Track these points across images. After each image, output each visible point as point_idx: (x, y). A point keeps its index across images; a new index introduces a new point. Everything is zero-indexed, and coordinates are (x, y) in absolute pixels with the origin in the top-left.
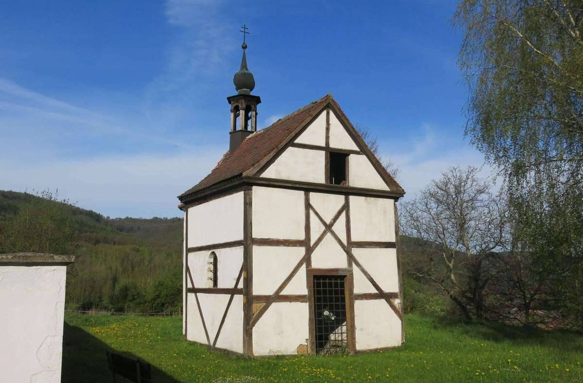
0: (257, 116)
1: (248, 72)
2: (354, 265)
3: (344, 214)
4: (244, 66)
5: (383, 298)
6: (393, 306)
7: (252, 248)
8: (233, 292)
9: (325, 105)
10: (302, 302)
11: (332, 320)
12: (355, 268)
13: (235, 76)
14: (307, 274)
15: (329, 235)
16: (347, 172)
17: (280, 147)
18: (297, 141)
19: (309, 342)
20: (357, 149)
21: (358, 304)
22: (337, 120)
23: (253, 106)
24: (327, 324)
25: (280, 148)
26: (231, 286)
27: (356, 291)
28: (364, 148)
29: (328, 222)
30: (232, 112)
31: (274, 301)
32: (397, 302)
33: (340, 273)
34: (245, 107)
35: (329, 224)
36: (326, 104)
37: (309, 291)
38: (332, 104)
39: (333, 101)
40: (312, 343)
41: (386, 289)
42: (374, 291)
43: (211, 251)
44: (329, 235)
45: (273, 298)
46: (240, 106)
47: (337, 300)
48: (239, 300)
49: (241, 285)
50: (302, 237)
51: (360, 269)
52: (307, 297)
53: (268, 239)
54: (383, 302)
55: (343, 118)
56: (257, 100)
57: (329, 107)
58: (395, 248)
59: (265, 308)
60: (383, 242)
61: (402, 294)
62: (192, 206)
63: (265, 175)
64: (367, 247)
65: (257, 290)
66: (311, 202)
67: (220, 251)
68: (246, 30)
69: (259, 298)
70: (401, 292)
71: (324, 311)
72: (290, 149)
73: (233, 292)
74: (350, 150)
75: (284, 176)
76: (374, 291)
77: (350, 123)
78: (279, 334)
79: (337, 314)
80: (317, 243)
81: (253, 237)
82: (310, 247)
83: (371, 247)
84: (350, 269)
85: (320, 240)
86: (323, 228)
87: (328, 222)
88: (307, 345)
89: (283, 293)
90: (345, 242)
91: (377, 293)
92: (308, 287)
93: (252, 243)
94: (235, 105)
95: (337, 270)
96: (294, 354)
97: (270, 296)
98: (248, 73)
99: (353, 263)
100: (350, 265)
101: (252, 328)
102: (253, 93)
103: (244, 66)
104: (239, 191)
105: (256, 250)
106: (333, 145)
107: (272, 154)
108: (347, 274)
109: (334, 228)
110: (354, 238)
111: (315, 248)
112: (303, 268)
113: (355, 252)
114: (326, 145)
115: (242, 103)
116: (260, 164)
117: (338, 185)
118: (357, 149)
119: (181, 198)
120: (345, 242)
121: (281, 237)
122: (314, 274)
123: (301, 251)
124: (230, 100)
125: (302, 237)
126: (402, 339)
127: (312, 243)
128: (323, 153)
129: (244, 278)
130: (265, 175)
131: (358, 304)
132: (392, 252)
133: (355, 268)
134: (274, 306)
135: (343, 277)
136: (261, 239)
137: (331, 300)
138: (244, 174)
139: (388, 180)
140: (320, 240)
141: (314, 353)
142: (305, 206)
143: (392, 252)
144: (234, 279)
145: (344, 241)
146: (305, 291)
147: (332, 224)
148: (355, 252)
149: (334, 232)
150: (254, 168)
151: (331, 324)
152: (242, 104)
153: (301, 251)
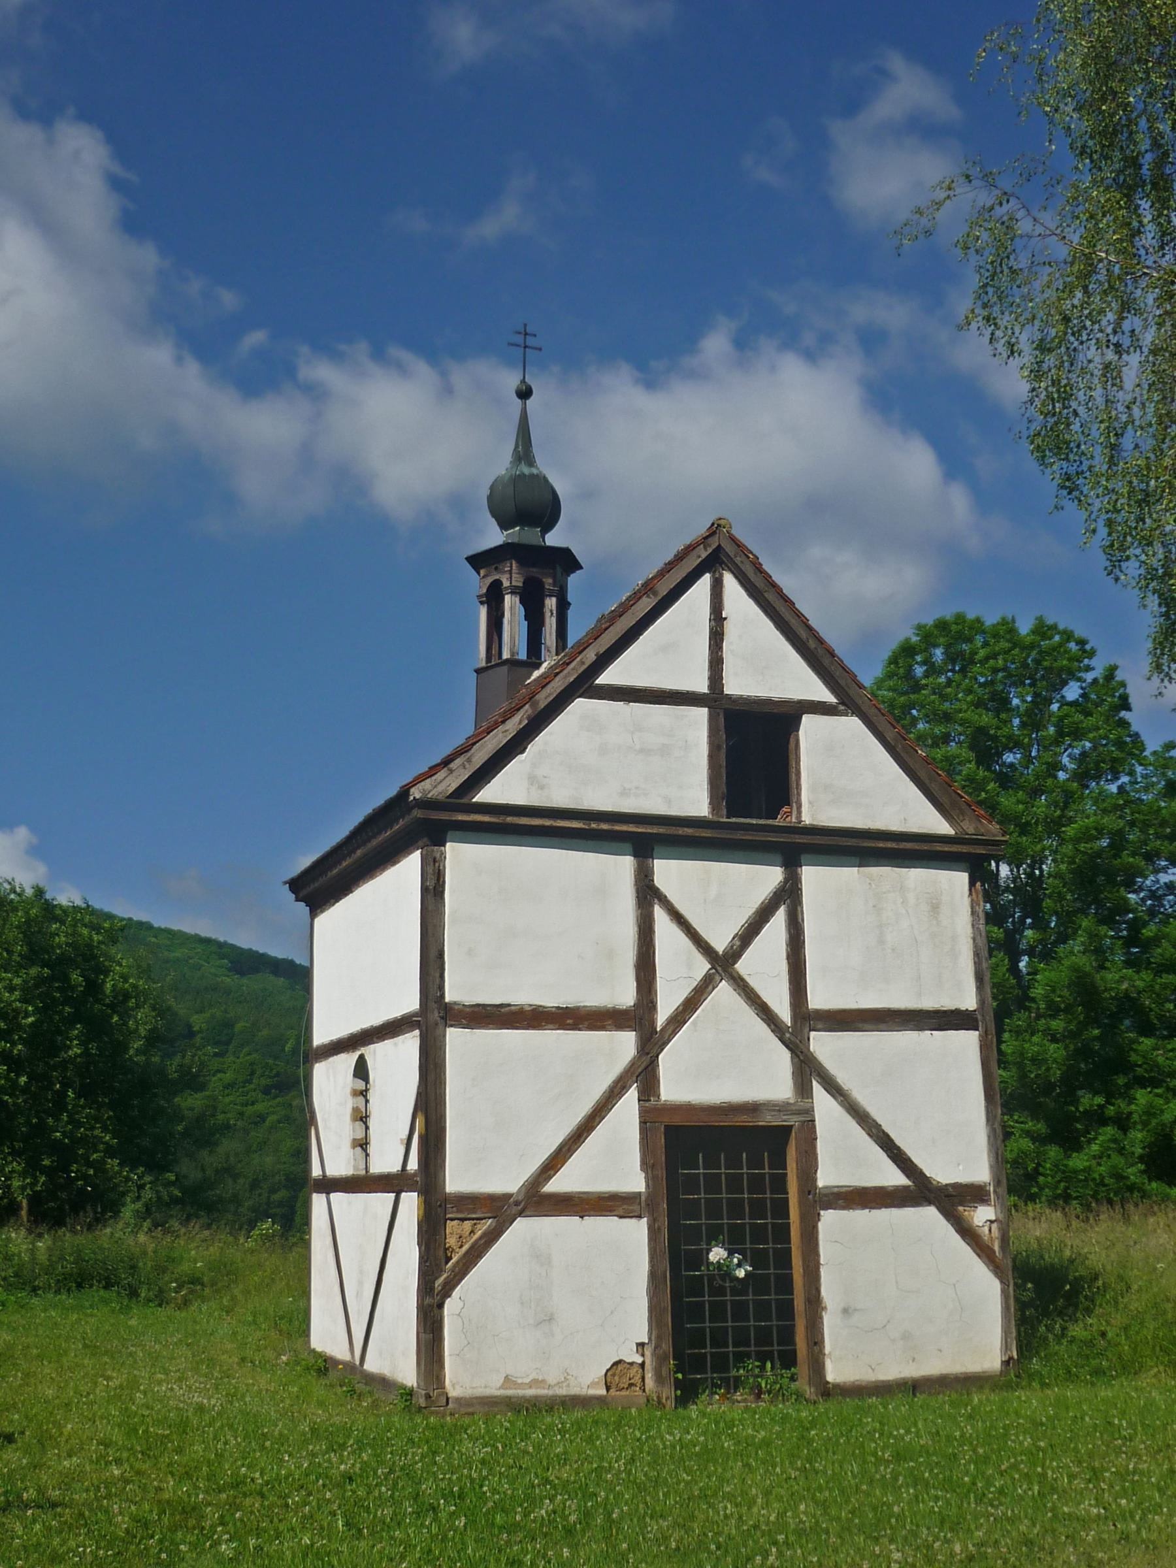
0: (570, 613)
1: (535, 471)
2: (817, 1088)
3: (779, 918)
4: (524, 451)
5: (930, 1202)
6: (967, 1232)
7: (444, 1036)
8: (392, 1183)
9: (704, 555)
10: (621, 1217)
11: (737, 1278)
12: (821, 1098)
13: (492, 488)
14: (643, 1123)
15: (724, 989)
16: (793, 777)
17: (544, 698)
18: (606, 678)
19: (648, 1353)
20: (826, 695)
21: (829, 1220)
22: (751, 602)
23: (548, 582)
24: (721, 1291)
25: (542, 705)
26: (394, 1167)
27: (825, 1178)
28: (851, 693)
29: (720, 945)
30: (482, 603)
31: (521, 1214)
32: (983, 1216)
33: (769, 1119)
34: (521, 584)
35: (725, 953)
36: (710, 550)
37: (651, 1180)
38: (729, 548)
39: (733, 540)
40: (660, 1360)
41: (942, 1173)
42: (895, 1178)
43: (354, 1057)
44: (724, 989)
45: (517, 1203)
46: (506, 583)
47: (758, 1209)
48: (411, 1202)
49: (413, 1165)
50: (626, 996)
51: (841, 1104)
52: (643, 1198)
53: (501, 1006)
54: (931, 1213)
55: (771, 596)
56: (566, 561)
57: (722, 563)
58: (977, 1029)
59: (492, 1237)
60: (928, 1012)
61: (1003, 1190)
62: (322, 912)
63: (491, 793)
64: (867, 1026)
65: (456, 1181)
66: (659, 881)
67: (375, 1051)
68: (531, 341)
69: (472, 1204)
70: (998, 1183)
71: (709, 1251)
72: (580, 706)
73: (392, 1183)
74: (800, 702)
75: (560, 797)
76: (895, 1178)
77: (798, 615)
78: (538, 1324)
79: (757, 1259)
80: (679, 1019)
81: (447, 999)
82: (656, 1029)
83: (881, 1026)
84: (803, 1104)
85: (691, 1005)
86: (702, 966)
87: (720, 945)
88: (643, 1365)
89: (557, 1185)
90: (784, 1013)
91: (906, 1188)
92: (646, 1165)
93: (444, 1018)
94: (490, 580)
95: (753, 1108)
96: (592, 1392)
97: (506, 1197)
98: (532, 476)
99: (814, 1083)
100: (803, 1089)
101: (441, 1306)
102: (553, 539)
103: (524, 451)
104: (412, 853)
105: (455, 1038)
106: (736, 685)
107: (513, 726)
108: (793, 1121)
109: (742, 966)
110: (818, 999)
111: (674, 1033)
112: (629, 1102)
113: (822, 1044)
114: (710, 687)
115: (510, 572)
116: (469, 760)
117: (770, 822)
118: (828, 697)
119: (296, 885)
120: (784, 1013)
121: (550, 1001)
122: (667, 1120)
123: (625, 1044)
124: (478, 561)
125: (626, 996)
126: (1006, 1347)
127: (662, 1017)
128: (701, 714)
129: (420, 1137)
130: (491, 793)
131: (829, 1220)
132: (968, 1042)
133: (821, 1098)
134: (522, 1229)
135: (784, 1132)
136: (478, 1005)
137: (736, 1208)
138: (416, 793)
139: (944, 800)
140: (691, 1005)
141: (669, 1393)
142: (638, 891)
143: (968, 1042)
144: (401, 1140)
145: (783, 1009)
146: (635, 1182)
147: (734, 954)
148: (822, 1044)
149: (742, 980)
150: (451, 771)
151: (735, 1292)
152: (511, 576)
153: (625, 1044)
